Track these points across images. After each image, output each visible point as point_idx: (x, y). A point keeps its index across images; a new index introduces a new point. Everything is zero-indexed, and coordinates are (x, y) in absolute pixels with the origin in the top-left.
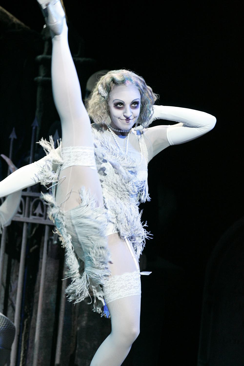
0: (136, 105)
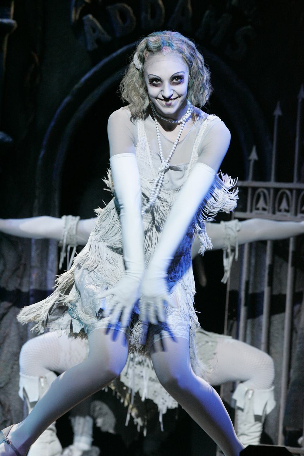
0: (179, 80)
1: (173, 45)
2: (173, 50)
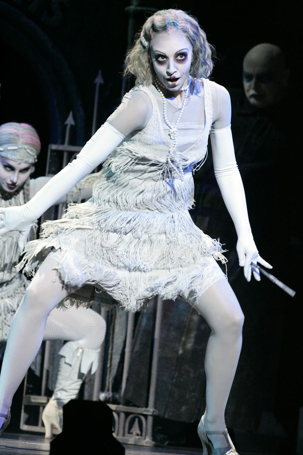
0: (184, 57)
1: (177, 25)
2: (178, 29)
